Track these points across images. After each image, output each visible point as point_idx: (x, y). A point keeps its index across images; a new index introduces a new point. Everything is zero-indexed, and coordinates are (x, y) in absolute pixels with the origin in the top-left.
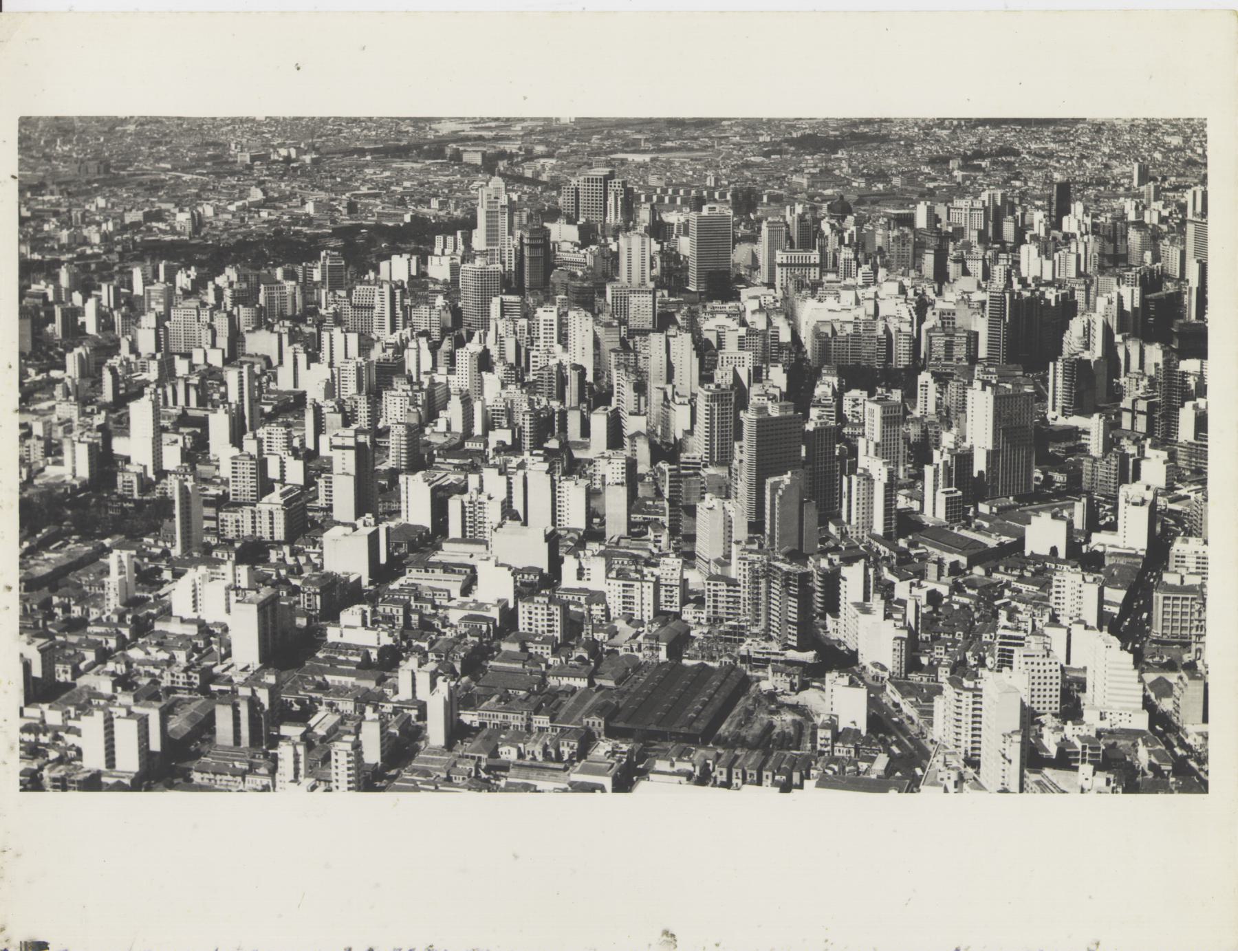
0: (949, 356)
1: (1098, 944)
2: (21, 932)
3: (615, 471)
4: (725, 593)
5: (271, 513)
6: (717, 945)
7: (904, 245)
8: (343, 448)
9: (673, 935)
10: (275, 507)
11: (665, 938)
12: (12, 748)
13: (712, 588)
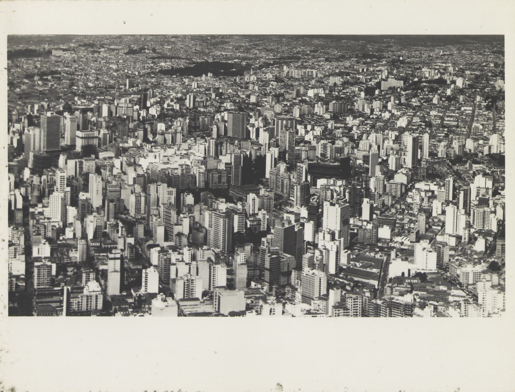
0: (220, 182)
1: (459, 389)
2: (7, 386)
3: (242, 258)
4: (343, 314)
5: (97, 296)
6: (300, 390)
7: (124, 126)
8: (115, 259)
9: (281, 386)
10: (98, 293)
11: (278, 386)
12: (5, 307)
13: (337, 312)
